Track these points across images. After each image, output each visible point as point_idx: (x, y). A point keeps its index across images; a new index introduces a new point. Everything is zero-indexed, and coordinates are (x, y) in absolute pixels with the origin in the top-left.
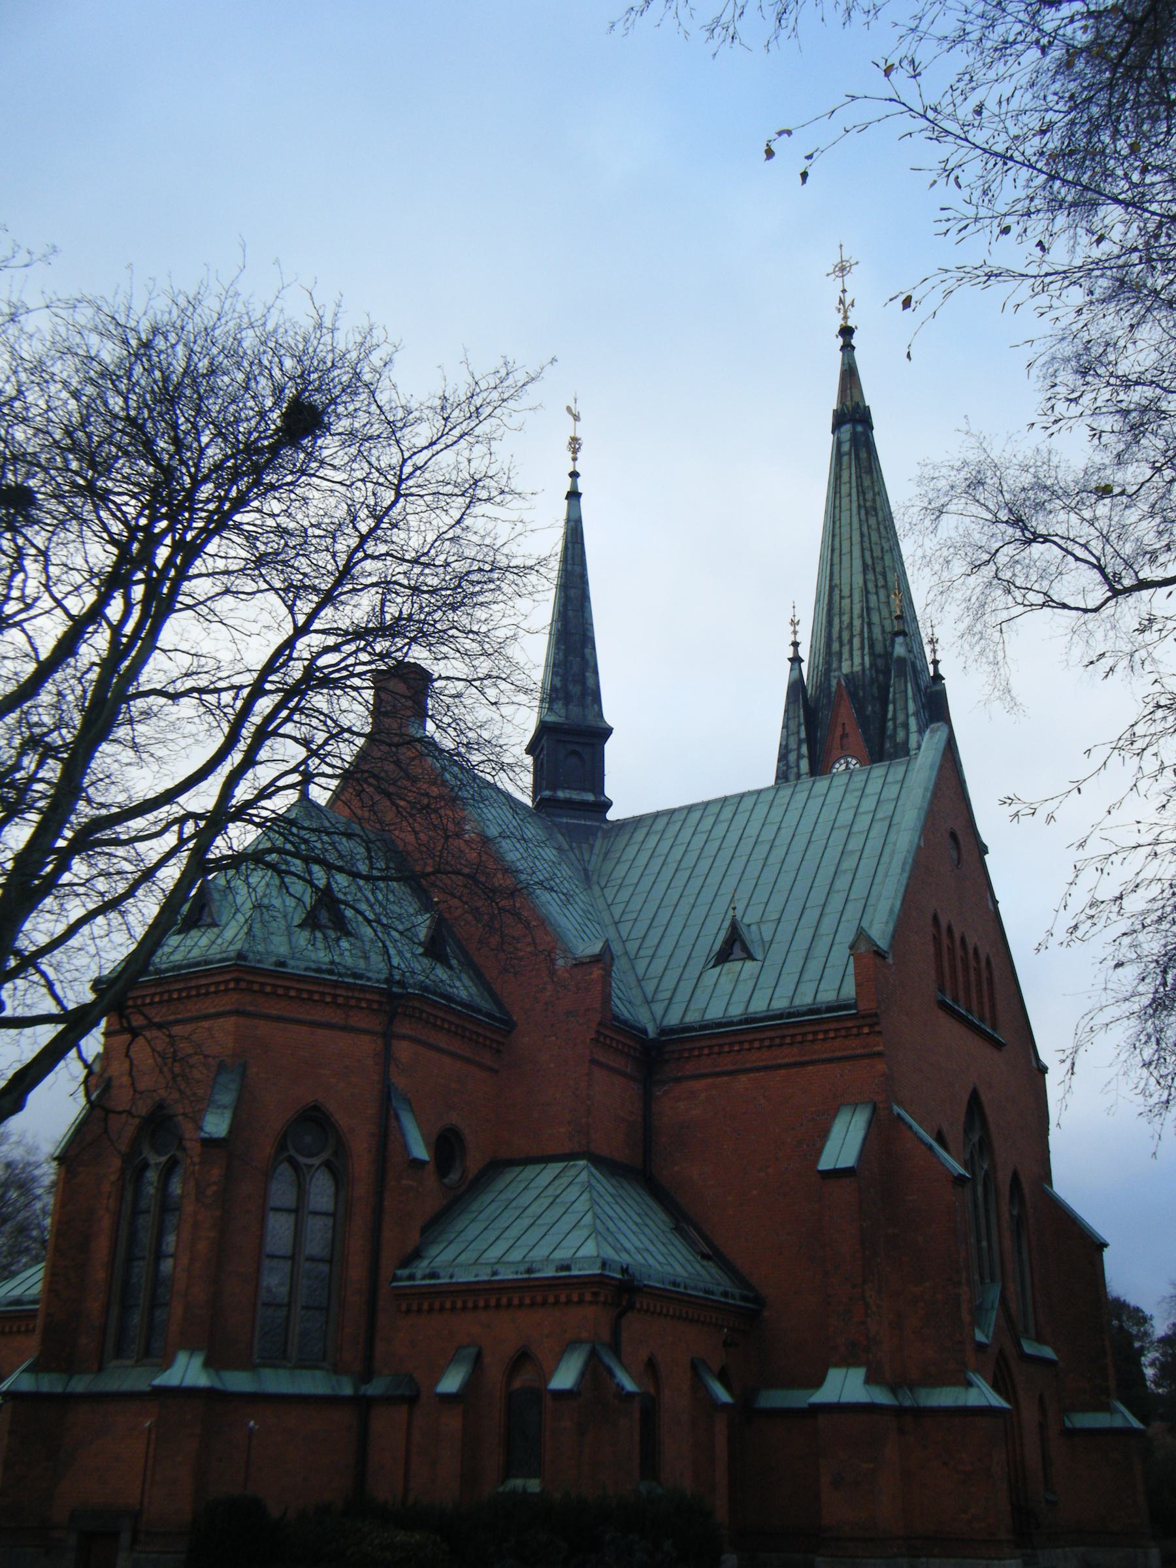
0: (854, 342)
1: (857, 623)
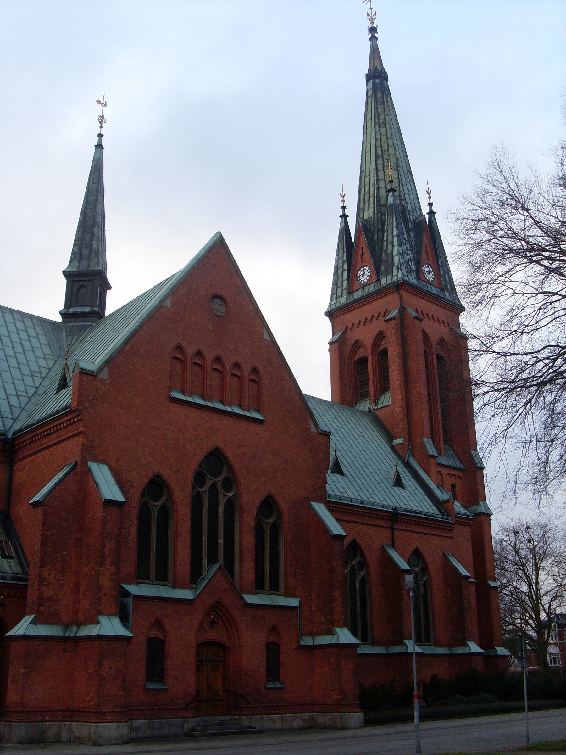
0: (376, 35)
1: (372, 189)
